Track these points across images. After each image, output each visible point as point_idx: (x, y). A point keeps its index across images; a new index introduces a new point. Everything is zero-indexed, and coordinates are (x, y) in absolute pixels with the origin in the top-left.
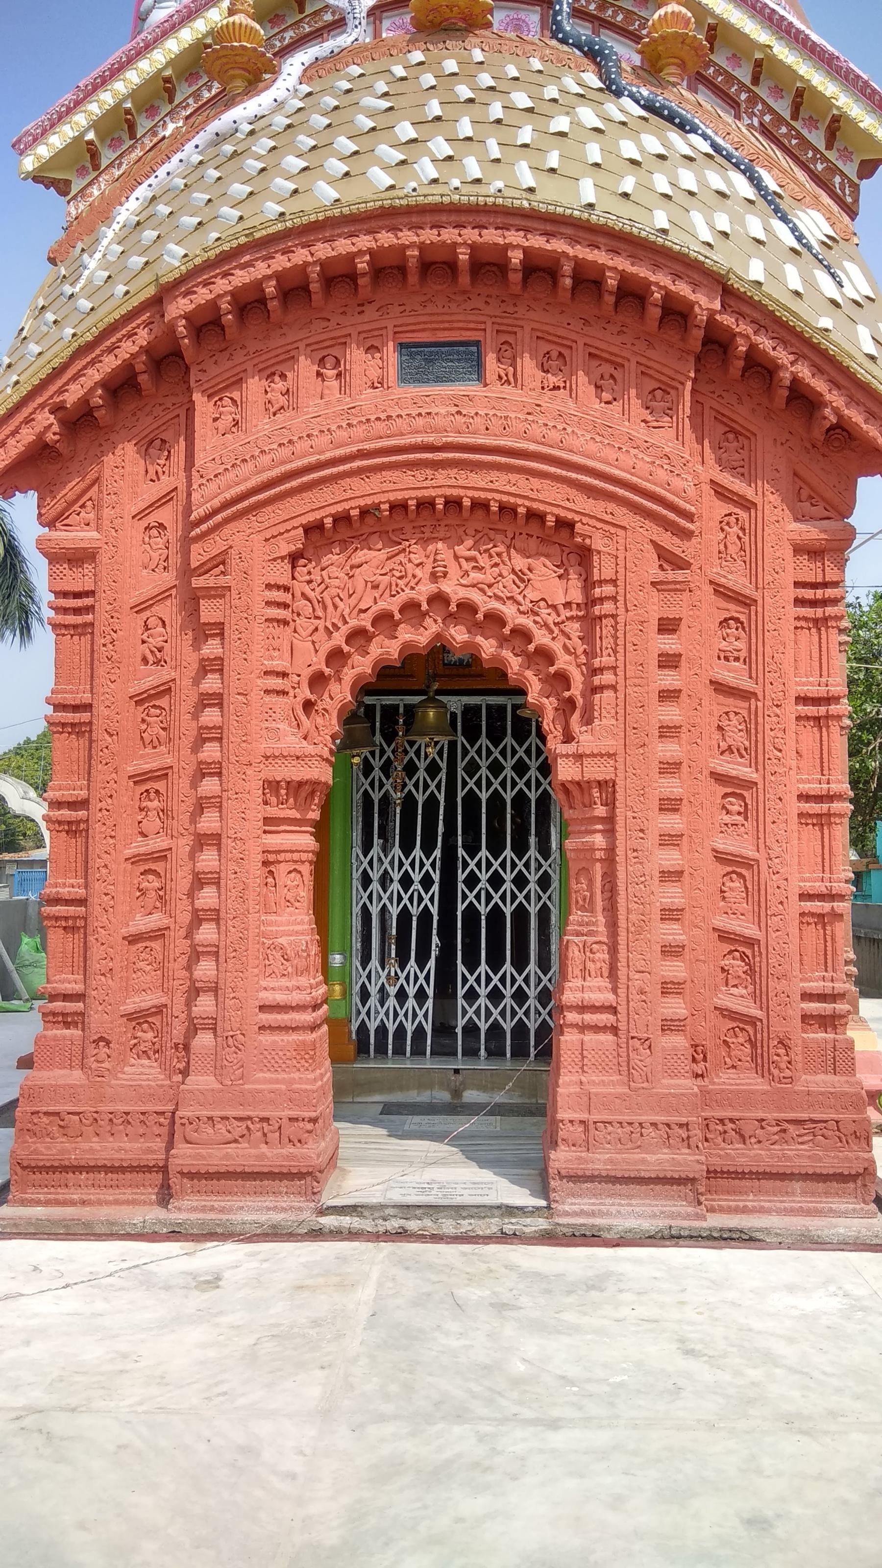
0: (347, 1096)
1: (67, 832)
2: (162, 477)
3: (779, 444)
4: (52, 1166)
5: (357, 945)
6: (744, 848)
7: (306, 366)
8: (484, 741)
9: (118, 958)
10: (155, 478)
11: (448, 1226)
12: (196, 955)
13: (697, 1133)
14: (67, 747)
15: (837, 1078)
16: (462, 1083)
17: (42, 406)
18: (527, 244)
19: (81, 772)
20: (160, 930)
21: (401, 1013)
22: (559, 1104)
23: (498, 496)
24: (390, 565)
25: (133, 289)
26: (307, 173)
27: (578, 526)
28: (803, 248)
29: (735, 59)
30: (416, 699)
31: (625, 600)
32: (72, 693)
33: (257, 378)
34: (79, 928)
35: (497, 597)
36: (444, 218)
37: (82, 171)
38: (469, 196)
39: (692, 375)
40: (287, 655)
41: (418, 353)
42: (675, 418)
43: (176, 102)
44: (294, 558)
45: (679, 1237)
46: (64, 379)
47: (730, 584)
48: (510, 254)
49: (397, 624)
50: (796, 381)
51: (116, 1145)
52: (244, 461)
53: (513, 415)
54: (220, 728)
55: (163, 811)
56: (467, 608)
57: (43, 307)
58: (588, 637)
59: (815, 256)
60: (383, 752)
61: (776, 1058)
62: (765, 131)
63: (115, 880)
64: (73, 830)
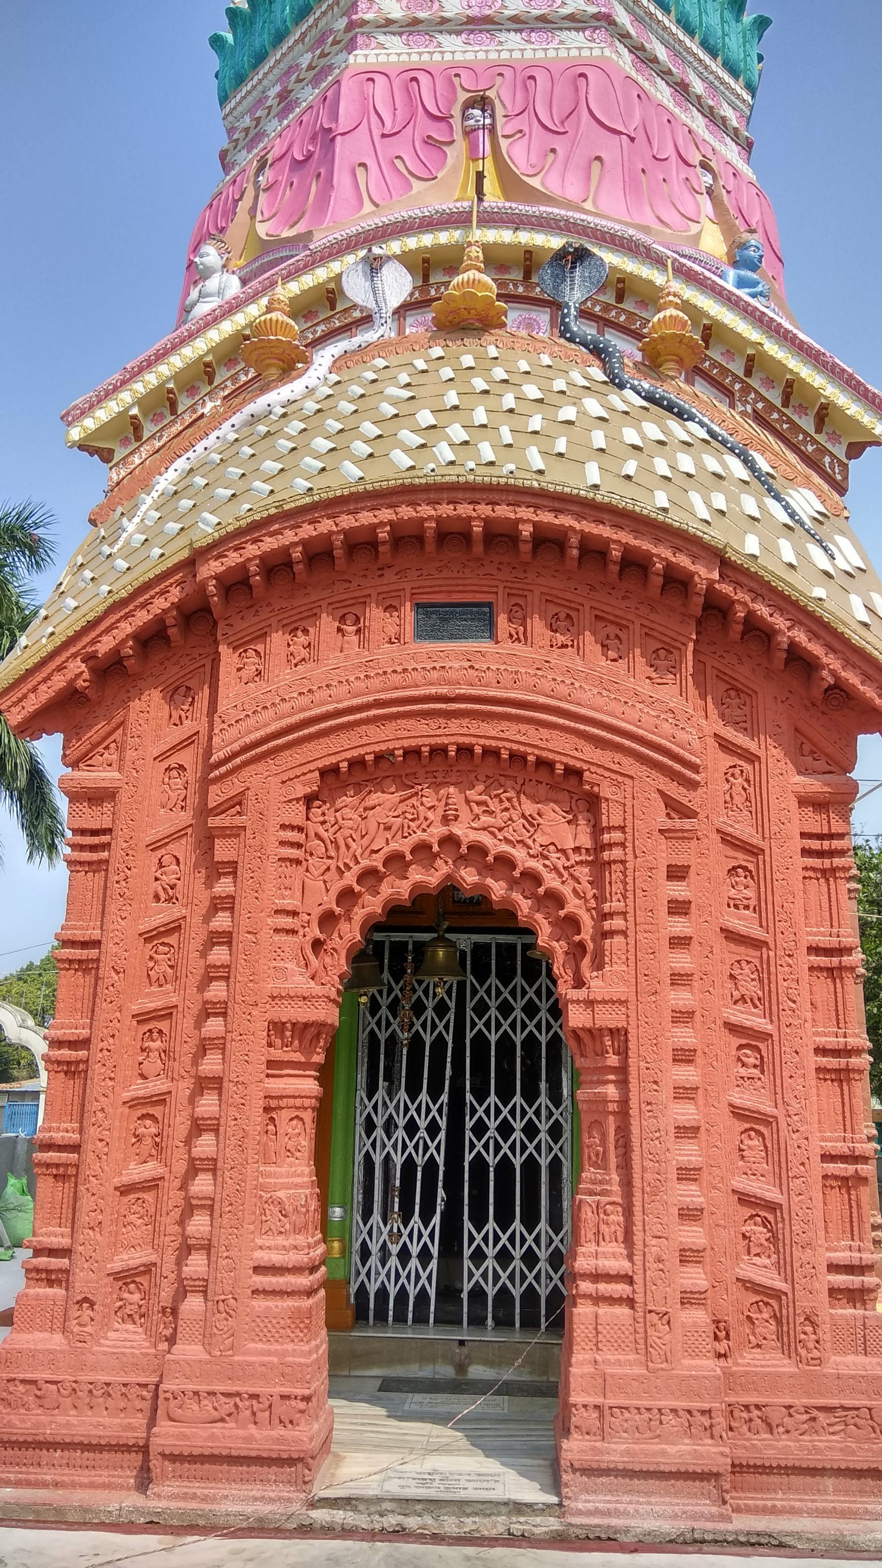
0: (342, 1366)
1: (66, 1073)
2: (185, 722)
3: (779, 701)
4: (25, 1442)
5: (358, 1197)
6: (762, 1103)
7: (327, 623)
8: (493, 980)
9: (108, 1210)
10: (178, 722)
11: (450, 1524)
12: (189, 1209)
13: (720, 1420)
14: (72, 985)
15: (867, 1360)
16: (468, 1356)
17: (74, 656)
18: (536, 519)
19: (85, 1010)
20: (154, 1180)
21: (403, 1274)
22: (572, 1386)
23: (508, 745)
24: (402, 808)
25: (168, 552)
26: (334, 453)
27: (586, 774)
28: (794, 525)
29: (729, 354)
30: (426, 937)
31: (634, 847)
32: (82, 929)
33: (280, 632)
34: (70, 1176)
35: (507, 841)
36: (460, 495)
37: (125, 442)
38: (484, 476)
39: (694, 637)
40: (298, 894)
41: (432, 613)
42: (678, 676)
43: (215, 384)
44: (309, 800)
45: (703, 1542)
46: (98, 631)
47: (737, 833)
48: (520, 527)
49: (408, 865)
50: (793, 644)
51: (95, 1420)
52: (265, 708)
53: (523, 670)
54: (228, 966)
55: (165, 1052)
56: (478, 849)
57: (82, 565)
58: (597, 882)
59: (808, 531)
60: (390, 990)
61: (803, 1336)
62: (760, 419)
63: (111, 1123)
64: (71, 1070)
